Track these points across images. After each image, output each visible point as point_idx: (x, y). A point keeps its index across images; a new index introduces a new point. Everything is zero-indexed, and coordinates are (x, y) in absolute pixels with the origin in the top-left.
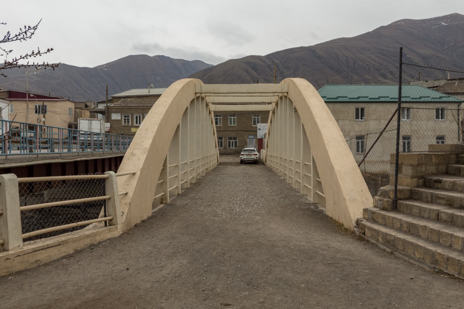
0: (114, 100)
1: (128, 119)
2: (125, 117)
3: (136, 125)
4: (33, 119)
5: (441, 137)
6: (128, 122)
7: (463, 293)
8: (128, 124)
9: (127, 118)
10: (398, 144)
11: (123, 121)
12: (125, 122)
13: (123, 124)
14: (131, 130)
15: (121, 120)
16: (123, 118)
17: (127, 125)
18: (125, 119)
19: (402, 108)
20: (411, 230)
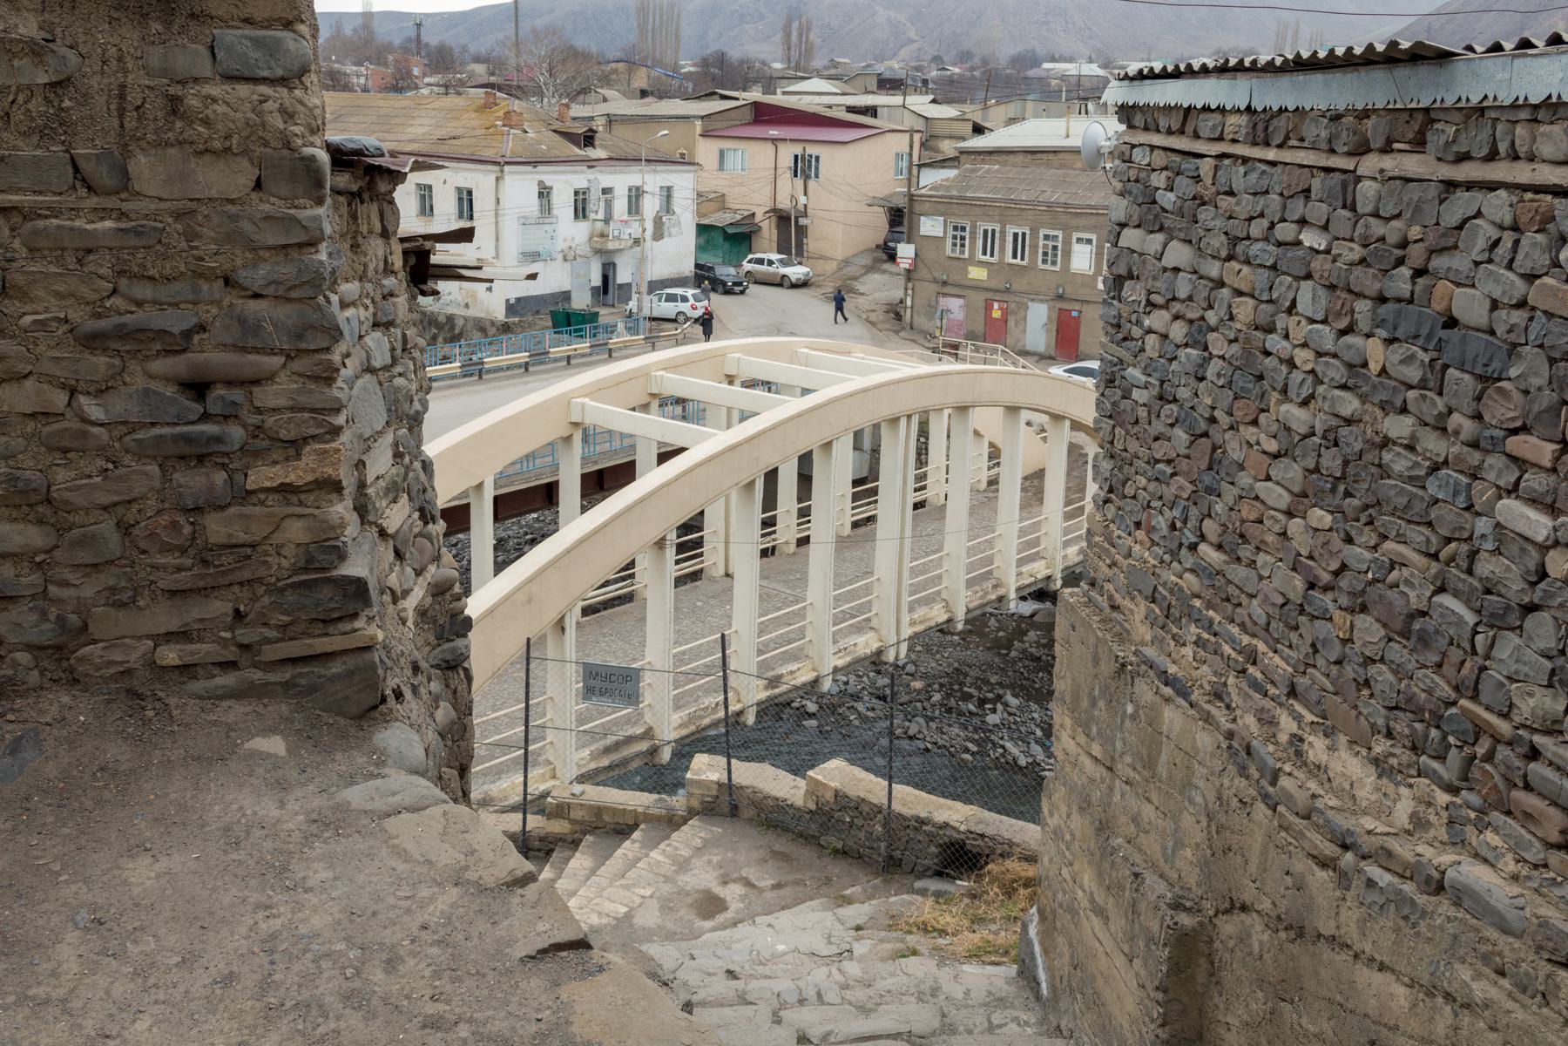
0: (963, 158)
1: (963, 238)
2: (956, 228)
3: (983, 258)
4: (788, 192)
5: (423, 197)
6: (963, 246)
7: (1559, 1043)
8: (962, 252)
9: (959, 233)
10: (817, 168)
11: (949, 241)
12: (955, 245)
13: (948, 252)
14: (967, 273)
15: (944, 238)
16: (951, 232)
17: (957, 255)
18: (955, 237)
19: (620, 286)
20: (760, 261)
